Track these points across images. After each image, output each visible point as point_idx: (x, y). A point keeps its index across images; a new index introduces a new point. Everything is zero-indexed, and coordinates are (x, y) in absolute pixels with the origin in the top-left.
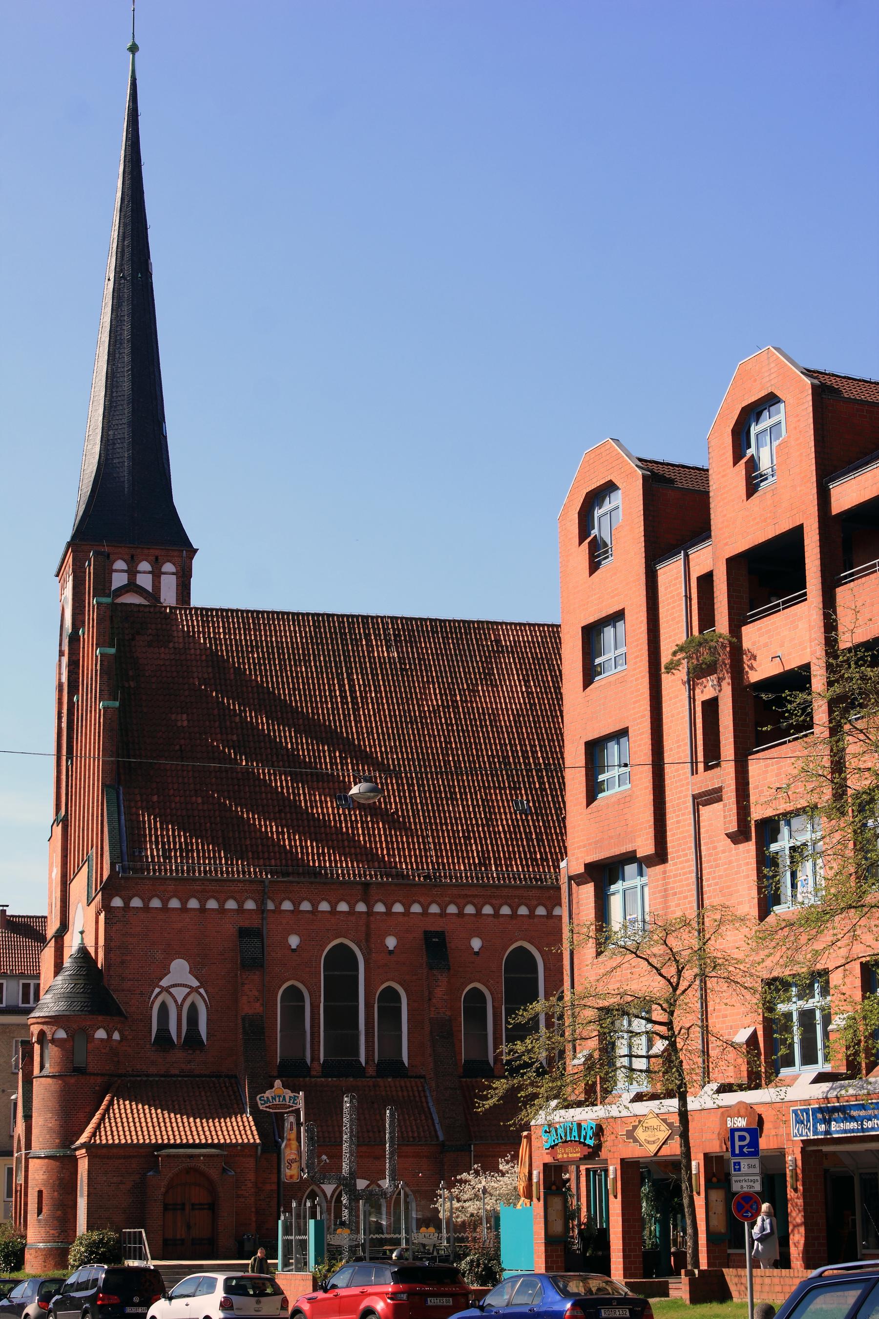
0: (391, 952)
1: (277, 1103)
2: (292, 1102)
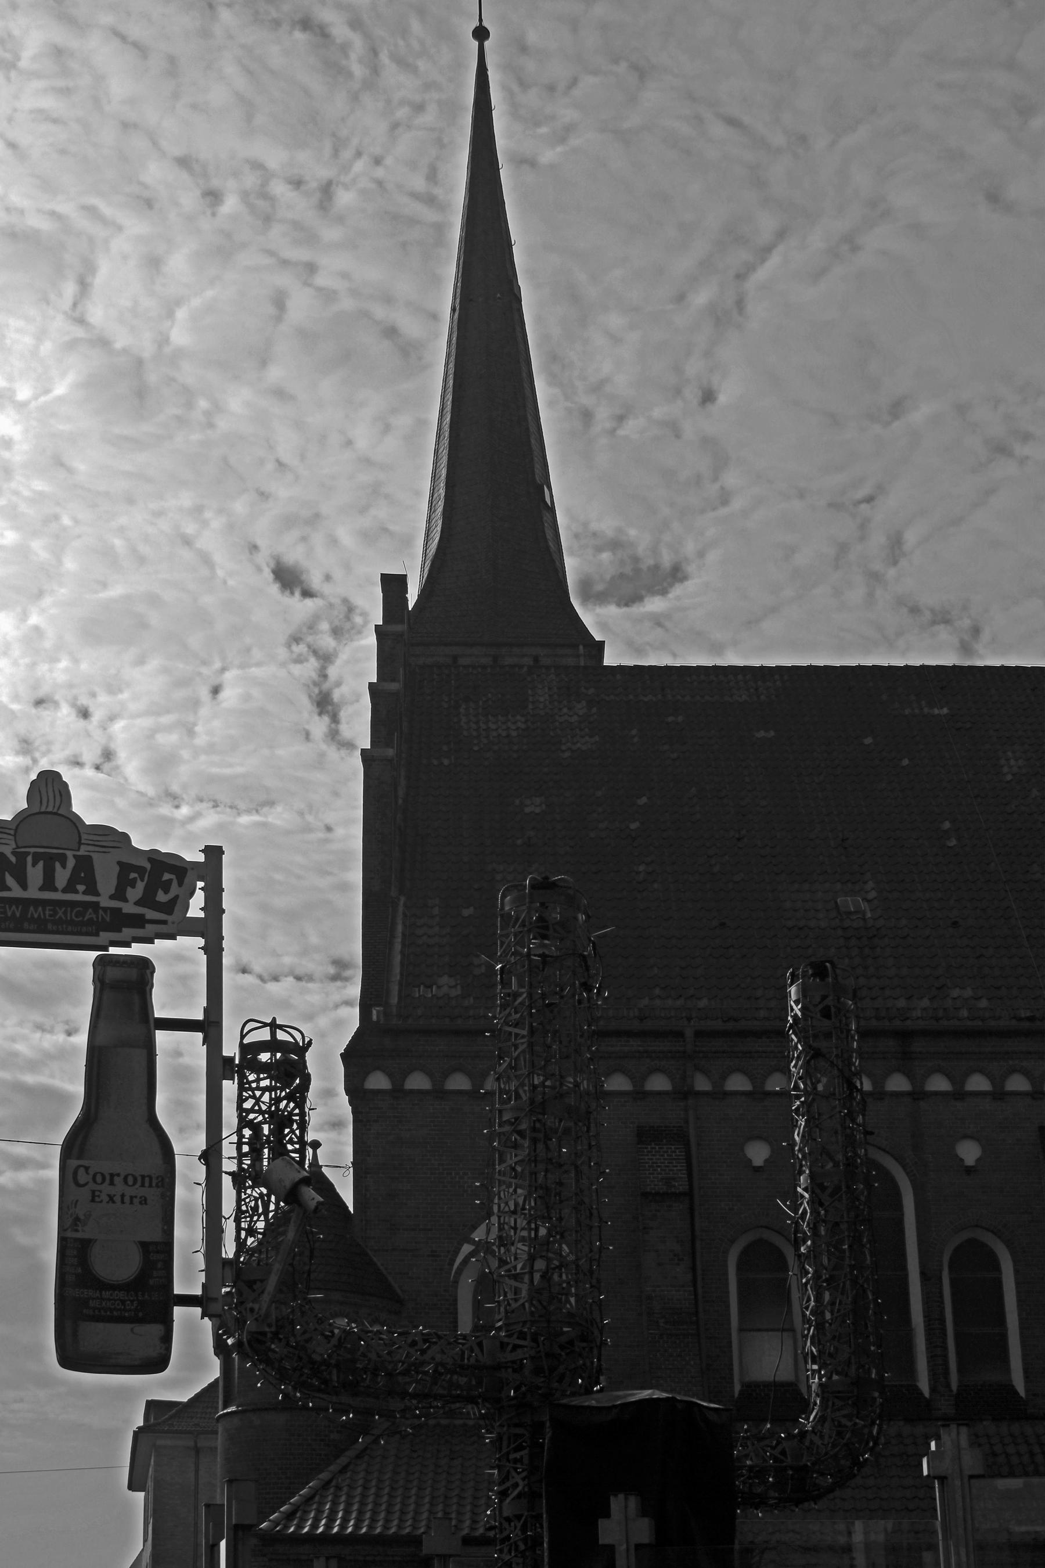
0: (969, 1170)
1: (33, 892)
2: (135, 893)
